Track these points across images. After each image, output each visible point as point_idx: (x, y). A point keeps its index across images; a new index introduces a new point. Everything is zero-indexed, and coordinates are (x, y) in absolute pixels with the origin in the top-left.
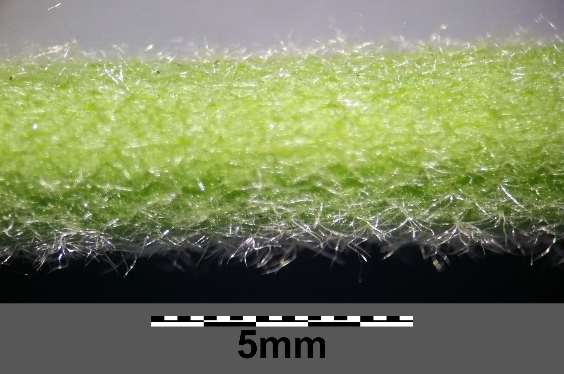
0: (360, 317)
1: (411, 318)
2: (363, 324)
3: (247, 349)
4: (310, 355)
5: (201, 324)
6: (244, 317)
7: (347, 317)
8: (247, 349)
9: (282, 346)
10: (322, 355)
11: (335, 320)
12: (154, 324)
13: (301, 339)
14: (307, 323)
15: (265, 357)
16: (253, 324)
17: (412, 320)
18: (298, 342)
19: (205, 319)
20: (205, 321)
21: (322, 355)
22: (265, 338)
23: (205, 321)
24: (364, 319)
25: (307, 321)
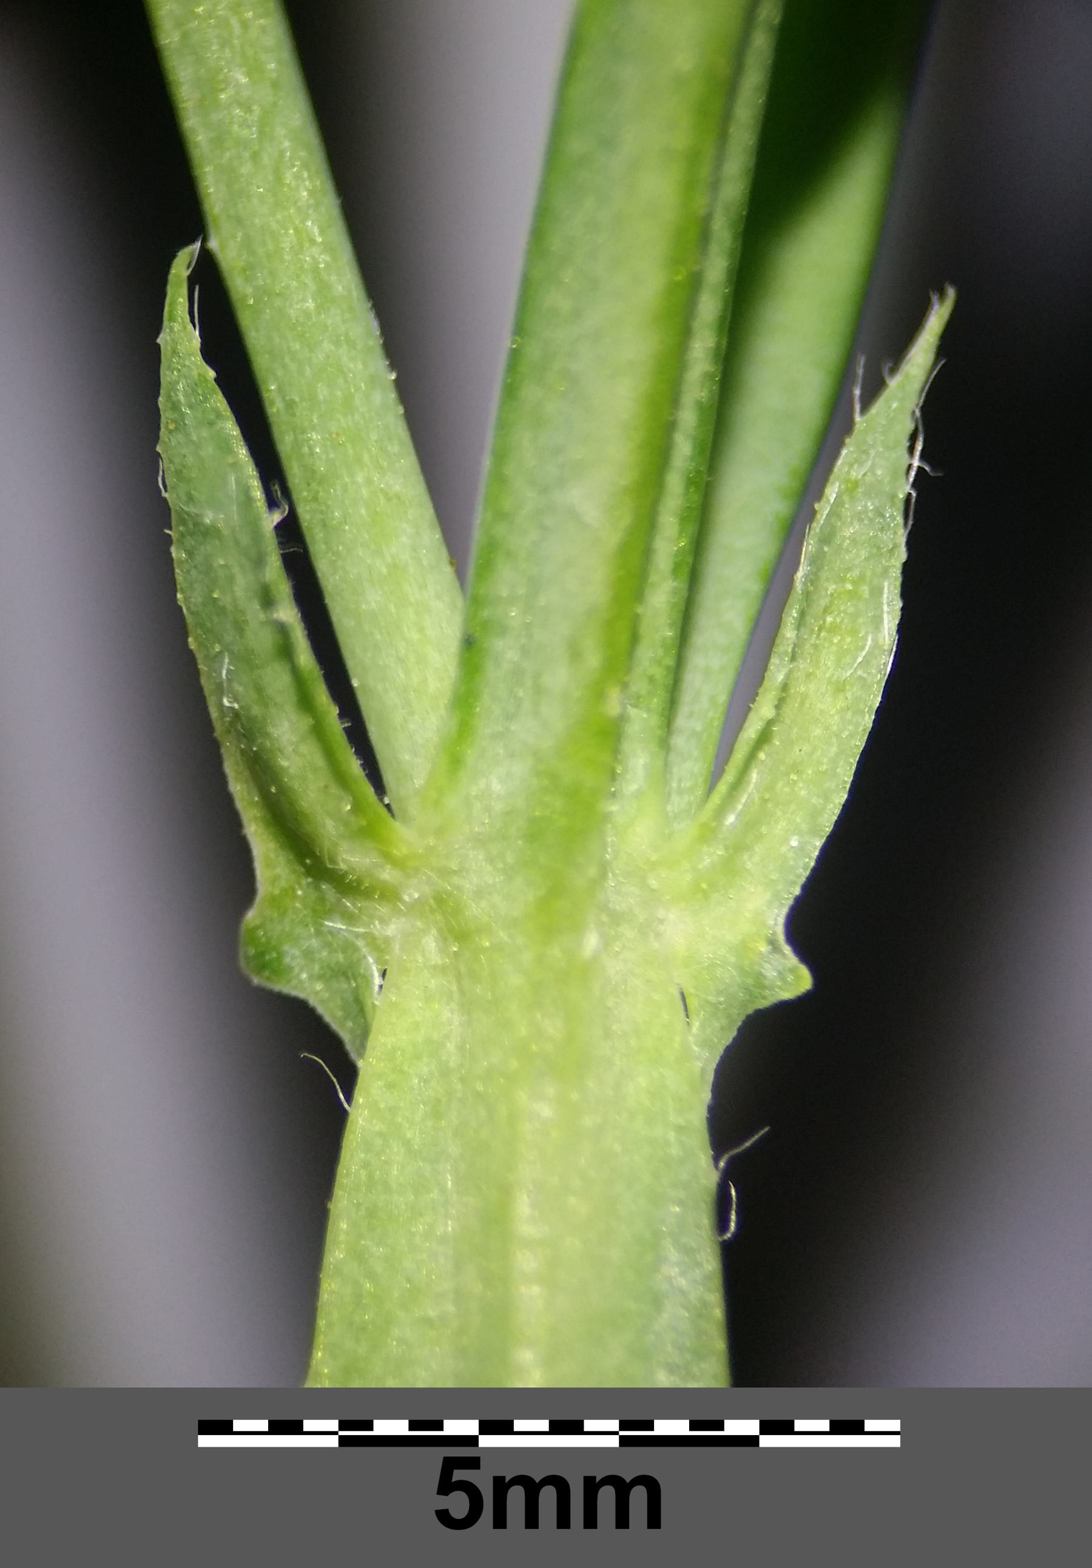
1: (895, 1425)
2: (768, 1441)
3: (458, 1504)
4: (622, 1521)
5: (613, 1442)
7: (442, 1422)
8: (458, 1504)
9: (548, 1497)
10: (654, 1521)
12: (206, 1441)
13: (507, 1480)
14: (336, 1437)
15: (536, 1527)
16: (472, 1441)
17: (898, 1429)
18: (591, 1486)
20: (342, 1433)
21: (654, 1521)
23: (622, 1433)
24: (768, 1428)
25: (616, 1433)
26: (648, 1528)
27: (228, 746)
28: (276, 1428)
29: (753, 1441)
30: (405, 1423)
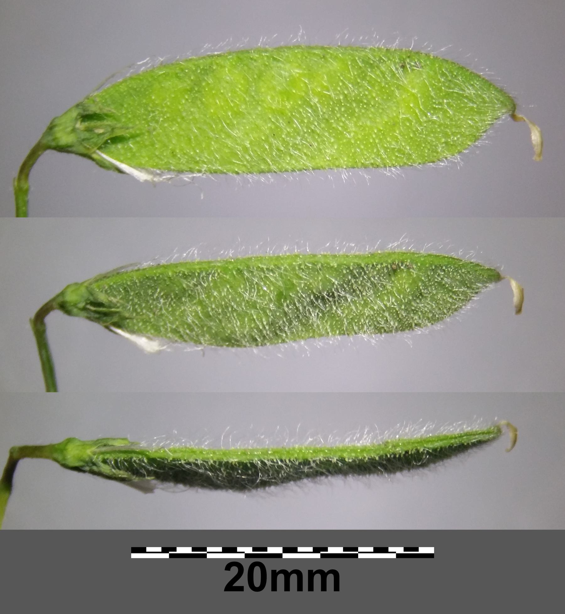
0: (282, 548)
2: (286, 556)
6: (420, 548)
9: (294, 579)
10: (337, 588)
11: (344, 551)
12: (134, 556)
13: (314, 572)
18: (311, 574)
19: (357, 554)
20: (357, 552)
21: (337, 588)
22: (312, 571)
23: (357, 552)
25: (208, 552)
26: (339, 591)
27: (384, 91)
28: (376, 550)
29: (280, 556)
30: (251, 548)
